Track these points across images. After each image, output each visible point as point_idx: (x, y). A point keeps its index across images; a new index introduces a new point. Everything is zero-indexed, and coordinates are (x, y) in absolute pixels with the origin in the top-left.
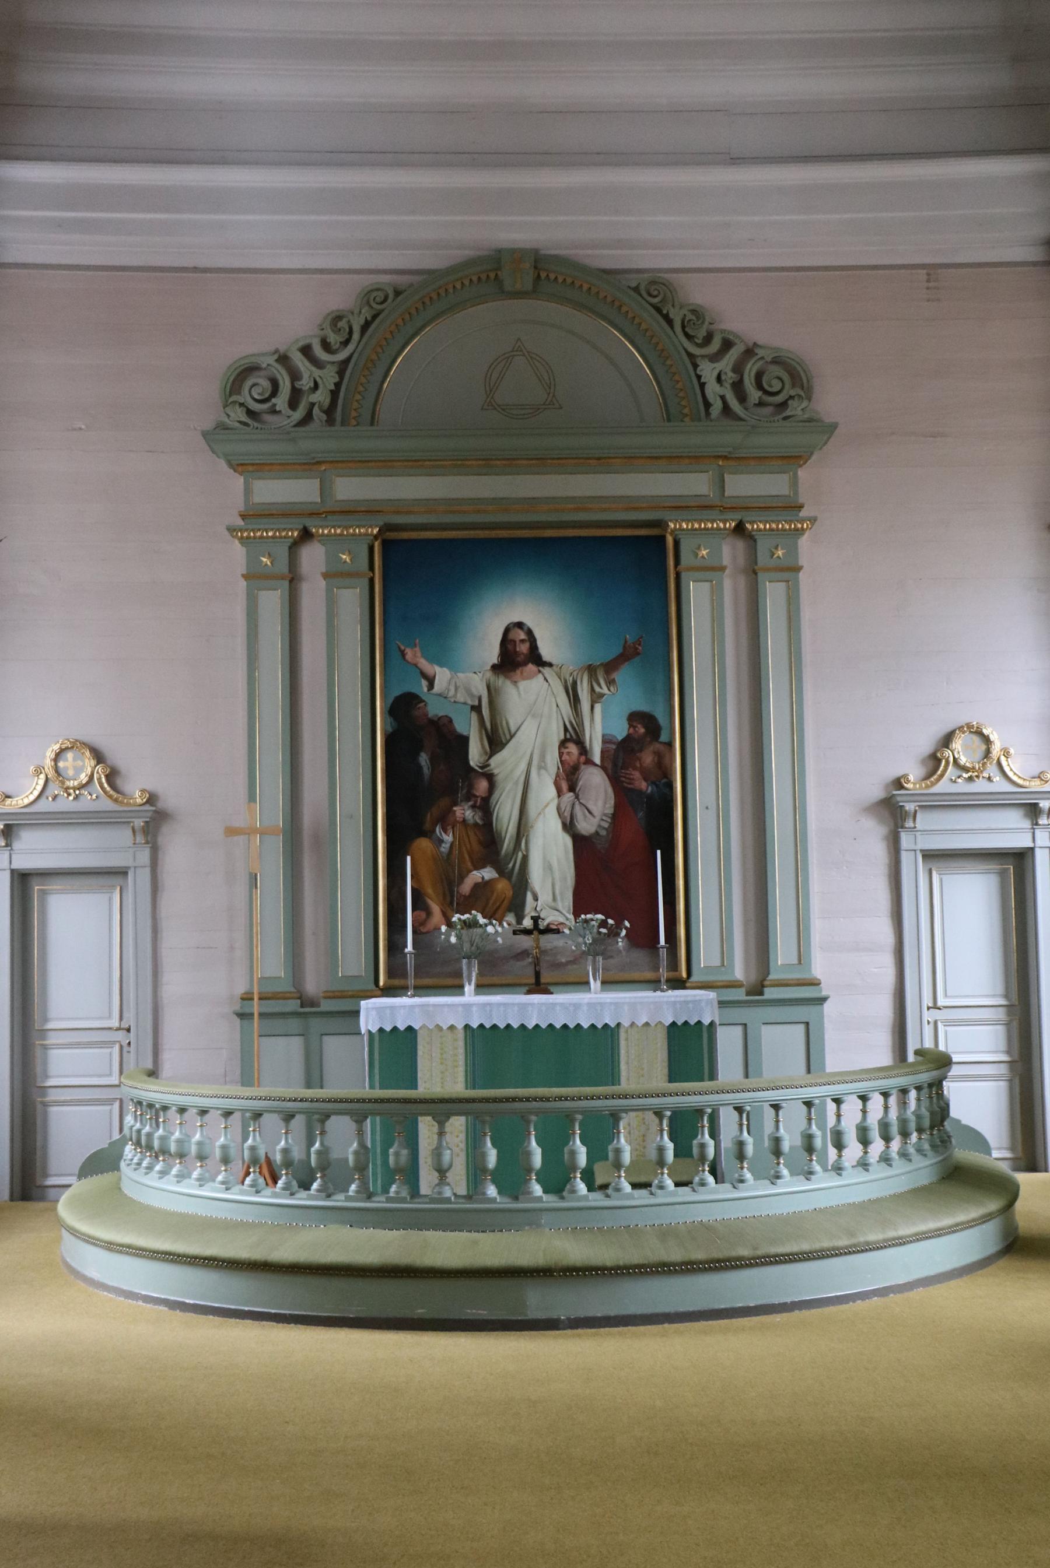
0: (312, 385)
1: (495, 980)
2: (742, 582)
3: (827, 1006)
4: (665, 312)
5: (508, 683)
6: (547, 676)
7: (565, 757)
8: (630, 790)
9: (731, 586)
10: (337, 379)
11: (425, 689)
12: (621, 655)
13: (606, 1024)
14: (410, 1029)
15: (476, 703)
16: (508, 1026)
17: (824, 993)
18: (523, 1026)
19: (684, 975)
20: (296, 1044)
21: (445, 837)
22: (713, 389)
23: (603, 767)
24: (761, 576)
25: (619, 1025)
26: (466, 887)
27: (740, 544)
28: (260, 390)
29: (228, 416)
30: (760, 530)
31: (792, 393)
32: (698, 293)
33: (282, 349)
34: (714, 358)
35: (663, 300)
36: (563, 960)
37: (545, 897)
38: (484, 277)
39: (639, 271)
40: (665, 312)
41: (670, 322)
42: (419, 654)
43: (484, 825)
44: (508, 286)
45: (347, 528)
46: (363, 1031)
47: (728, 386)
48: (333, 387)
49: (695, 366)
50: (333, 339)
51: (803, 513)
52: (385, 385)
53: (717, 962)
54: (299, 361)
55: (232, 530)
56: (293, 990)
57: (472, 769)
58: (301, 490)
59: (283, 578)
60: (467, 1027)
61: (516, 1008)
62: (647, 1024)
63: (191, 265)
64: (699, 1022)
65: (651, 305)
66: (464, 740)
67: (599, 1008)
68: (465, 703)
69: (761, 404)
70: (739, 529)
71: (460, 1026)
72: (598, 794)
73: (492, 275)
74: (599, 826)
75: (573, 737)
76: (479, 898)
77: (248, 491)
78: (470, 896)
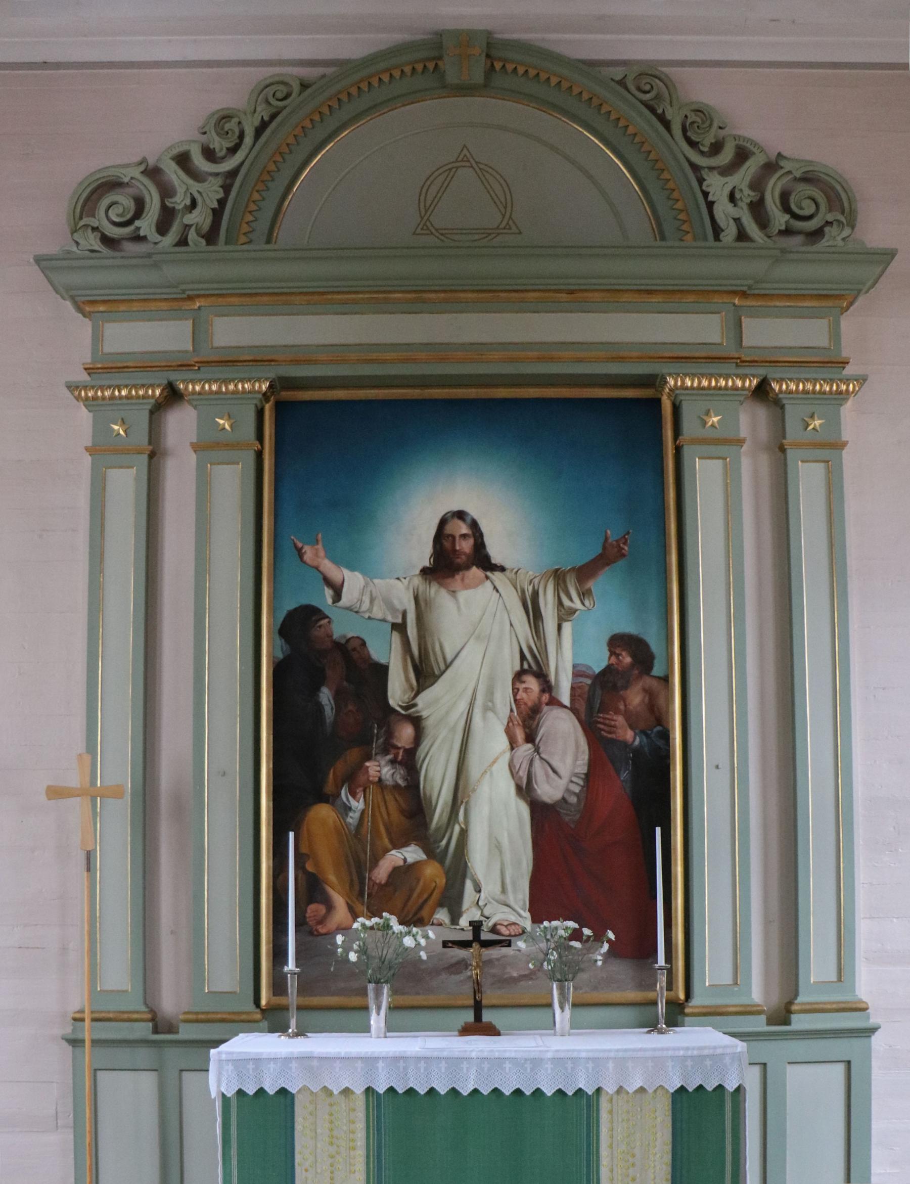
0: (188, 202)
1: (420, 1000)
2: (764, 460)
3: (876, 1040)
4: (660, 111)
5: (443, 592)
6: (497, 584)
7: (521, 695)
8: (614, 742)
9: (751, 467)
10: (221, 195)
11: (330, 601)
12: (601, 556)
13: (580, 1089)
14: (283, 1092)
15: (399, 620)
16: (432, 1091)
17: (873, 1021)
18: (454, 1091)
19: (682, 996)
20: (147, 1082)
21: (353, 803)
22: (724, 210)
23: (573, 710)
24: (790, 454)
25: (599, 1090)
26: (382, 872)
27: (762, 413)
28: (120, 210)
29: (77, 243)
30: (791, 392)
31: (830, 218)
32: (701, 89)
33: (151, 162)
34: (727, 171)
35: (658, 97)
36: (515, 974)
37: (491, 887)
38: (419, 67)
39: (625, 63)
40: (660, 111)
41: (667, 124)
42: (322, 553)
43: (407, 787)
44: (452, 77)
45: (226, 382)
46: (214, 1094)
47: (745, 207)
48: (215, 205)
49: (701, 181)
50: (219, 144)
51: (849, 370)
52: (286, 203)
53: (728, 979)
54: (174, 174)
55: (72, 387)
56: (143, 1008)
57: (394, 711)
58: (167, 336)
59: (140, 452)
60: (369, 1091)
61: (443, 1065)
62: (642, 1090)
63: (39, 59)
64: (720, 1087)
65: (642, 102)
66: (382, 671)
67: (569, 1065)
68: (384, 620)
69: (787, 232)
70: (762, 392)
71: (359, 1090)
72: (566, 748)
73: (431, 66)
74: (568, 790)
75: (532, 667)
76: (406, 899)
77: (97, 338)
78: (387, 884)
